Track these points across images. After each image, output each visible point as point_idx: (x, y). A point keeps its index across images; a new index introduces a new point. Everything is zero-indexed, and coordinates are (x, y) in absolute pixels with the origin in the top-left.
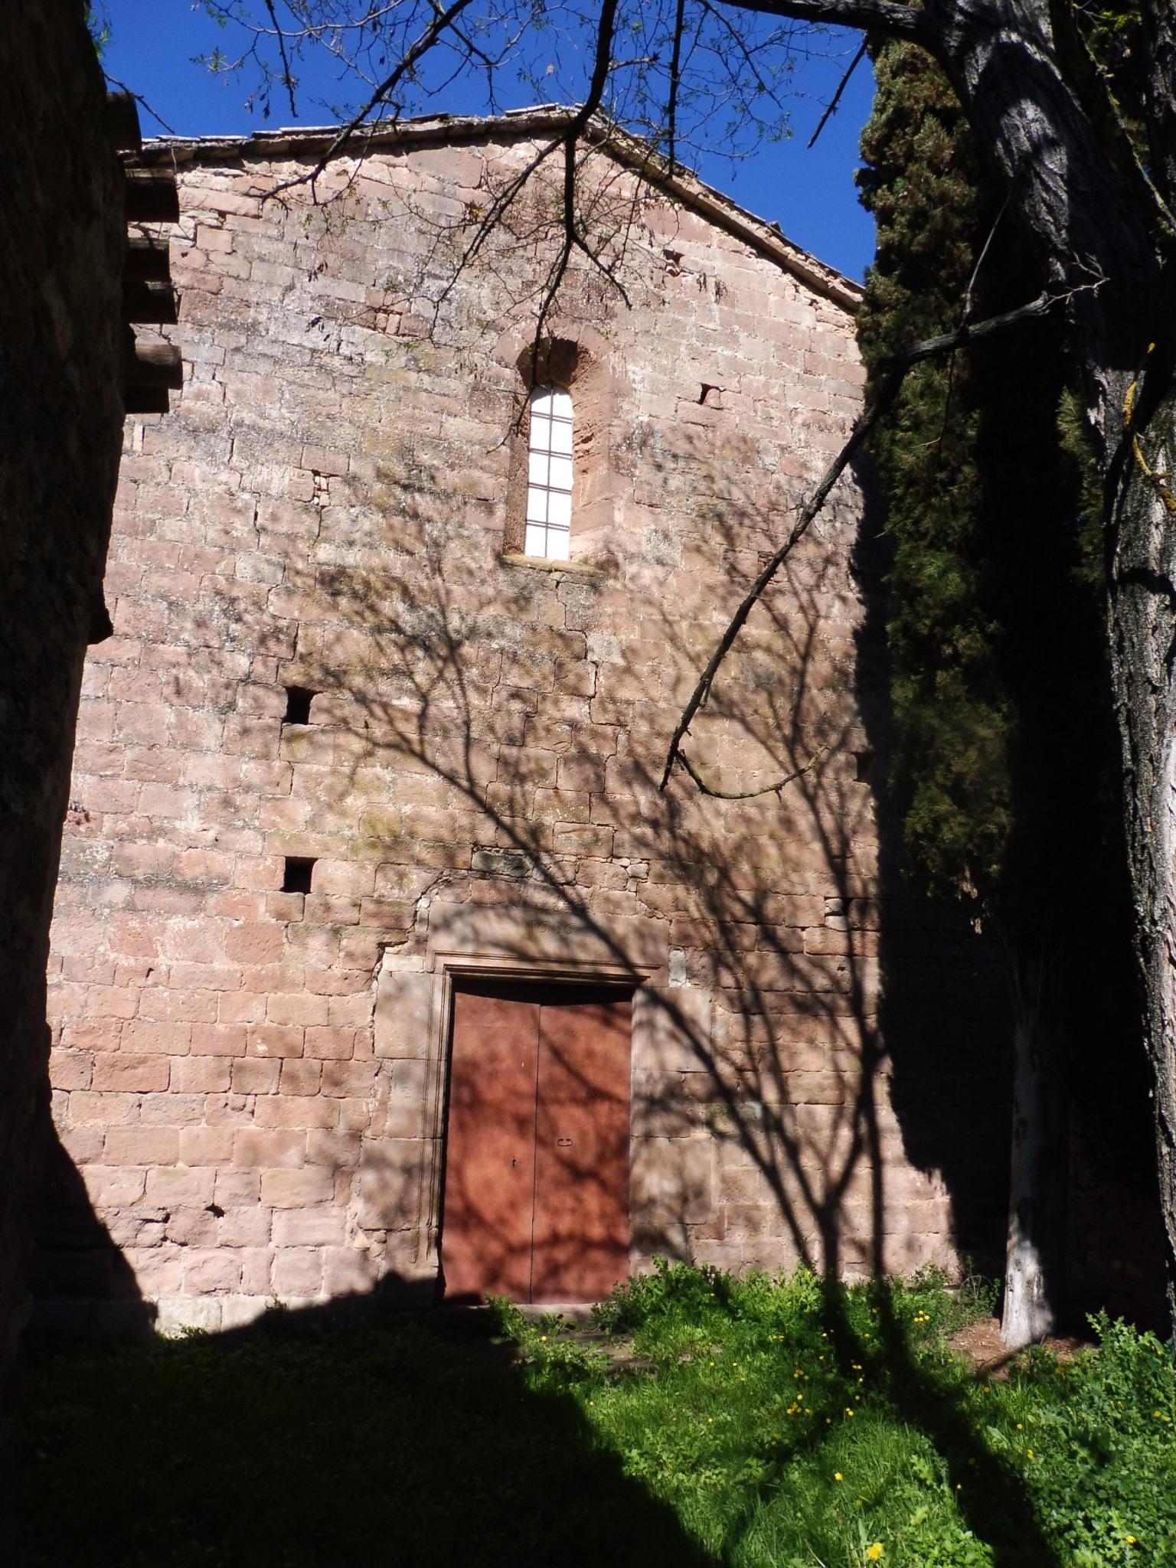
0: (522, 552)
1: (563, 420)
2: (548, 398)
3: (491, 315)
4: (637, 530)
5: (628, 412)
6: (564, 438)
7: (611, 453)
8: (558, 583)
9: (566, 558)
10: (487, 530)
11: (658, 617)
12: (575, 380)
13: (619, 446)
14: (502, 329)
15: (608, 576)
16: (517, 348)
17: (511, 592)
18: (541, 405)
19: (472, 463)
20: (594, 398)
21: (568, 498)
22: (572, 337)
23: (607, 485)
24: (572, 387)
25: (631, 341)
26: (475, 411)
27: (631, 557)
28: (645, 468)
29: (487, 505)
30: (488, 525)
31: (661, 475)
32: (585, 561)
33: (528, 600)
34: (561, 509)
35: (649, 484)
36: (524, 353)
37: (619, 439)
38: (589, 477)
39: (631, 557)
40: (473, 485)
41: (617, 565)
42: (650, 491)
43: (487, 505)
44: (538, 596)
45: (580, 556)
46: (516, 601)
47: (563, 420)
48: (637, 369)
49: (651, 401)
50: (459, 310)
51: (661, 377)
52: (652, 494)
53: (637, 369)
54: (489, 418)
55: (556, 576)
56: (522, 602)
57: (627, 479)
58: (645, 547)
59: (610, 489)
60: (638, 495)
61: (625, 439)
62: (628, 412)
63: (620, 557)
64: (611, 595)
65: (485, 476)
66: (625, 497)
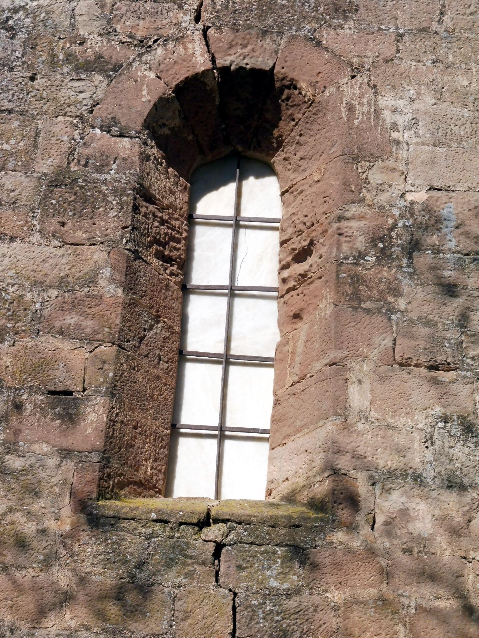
0: (167, 492)
1: (262, 224)
2: (232, 187)
3: (96, 44)
4: (401, 421)
5: (381, 188)
6: (261, 259)
7: (344, 278)
8: (219, 547)
9: (260, 496)
10: (65, 453)
11: (448, 604)
12: (280, 144)
13: (361, 255)
14: (117, 68)
15: (335, 524)
16: (146, 98)
17: (105, 578)
18: (216, 202)
19: (40, 324)
20: (314, 169)
21: (269, 374)
22: (263, 62)
23: (336, 336)
24: (277, 159)
25: (388, 51)
26: (53, 224)
27: (384, 480)
28: (420, 294)
29: (64, 402)
30: (66, 443)
31: (458, 303)
32: (290, 498)
33: (145, 590)
34: (254, 397)
35: (428, 323)
36: (161, 104)
37: (361, 243)
38: (303, 327)
39: (384, 480)
40: (41, 366)
41: (353, 501)
42: (431, 338)
43: (64, 402)
44: (170, 580)
45: (284, 488)
46: (119, 594)
47: (262, 224)
48: (401, 103)
49: (433, 161)
50: (32, 44)
51: (458, 111)
52: (435, 341)
53: (401, 103)
54: (81, 235)
55: (214, 532)
56: (131, 598)
57: (379, 320)
58: (419, 457)
59: (339, 345)
60: (404, 348)
61: (373, 242)
62: (381, 188)
63: (362, 488)
64: (337, 566)
65: (68, 345)
66: (374, 355)
